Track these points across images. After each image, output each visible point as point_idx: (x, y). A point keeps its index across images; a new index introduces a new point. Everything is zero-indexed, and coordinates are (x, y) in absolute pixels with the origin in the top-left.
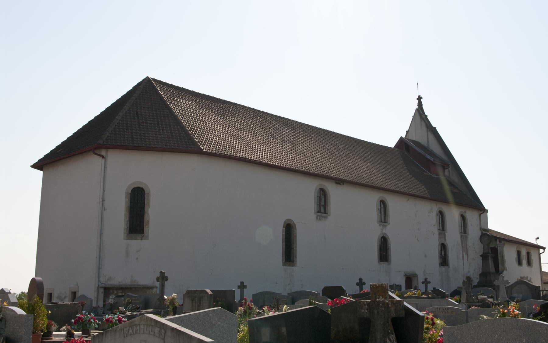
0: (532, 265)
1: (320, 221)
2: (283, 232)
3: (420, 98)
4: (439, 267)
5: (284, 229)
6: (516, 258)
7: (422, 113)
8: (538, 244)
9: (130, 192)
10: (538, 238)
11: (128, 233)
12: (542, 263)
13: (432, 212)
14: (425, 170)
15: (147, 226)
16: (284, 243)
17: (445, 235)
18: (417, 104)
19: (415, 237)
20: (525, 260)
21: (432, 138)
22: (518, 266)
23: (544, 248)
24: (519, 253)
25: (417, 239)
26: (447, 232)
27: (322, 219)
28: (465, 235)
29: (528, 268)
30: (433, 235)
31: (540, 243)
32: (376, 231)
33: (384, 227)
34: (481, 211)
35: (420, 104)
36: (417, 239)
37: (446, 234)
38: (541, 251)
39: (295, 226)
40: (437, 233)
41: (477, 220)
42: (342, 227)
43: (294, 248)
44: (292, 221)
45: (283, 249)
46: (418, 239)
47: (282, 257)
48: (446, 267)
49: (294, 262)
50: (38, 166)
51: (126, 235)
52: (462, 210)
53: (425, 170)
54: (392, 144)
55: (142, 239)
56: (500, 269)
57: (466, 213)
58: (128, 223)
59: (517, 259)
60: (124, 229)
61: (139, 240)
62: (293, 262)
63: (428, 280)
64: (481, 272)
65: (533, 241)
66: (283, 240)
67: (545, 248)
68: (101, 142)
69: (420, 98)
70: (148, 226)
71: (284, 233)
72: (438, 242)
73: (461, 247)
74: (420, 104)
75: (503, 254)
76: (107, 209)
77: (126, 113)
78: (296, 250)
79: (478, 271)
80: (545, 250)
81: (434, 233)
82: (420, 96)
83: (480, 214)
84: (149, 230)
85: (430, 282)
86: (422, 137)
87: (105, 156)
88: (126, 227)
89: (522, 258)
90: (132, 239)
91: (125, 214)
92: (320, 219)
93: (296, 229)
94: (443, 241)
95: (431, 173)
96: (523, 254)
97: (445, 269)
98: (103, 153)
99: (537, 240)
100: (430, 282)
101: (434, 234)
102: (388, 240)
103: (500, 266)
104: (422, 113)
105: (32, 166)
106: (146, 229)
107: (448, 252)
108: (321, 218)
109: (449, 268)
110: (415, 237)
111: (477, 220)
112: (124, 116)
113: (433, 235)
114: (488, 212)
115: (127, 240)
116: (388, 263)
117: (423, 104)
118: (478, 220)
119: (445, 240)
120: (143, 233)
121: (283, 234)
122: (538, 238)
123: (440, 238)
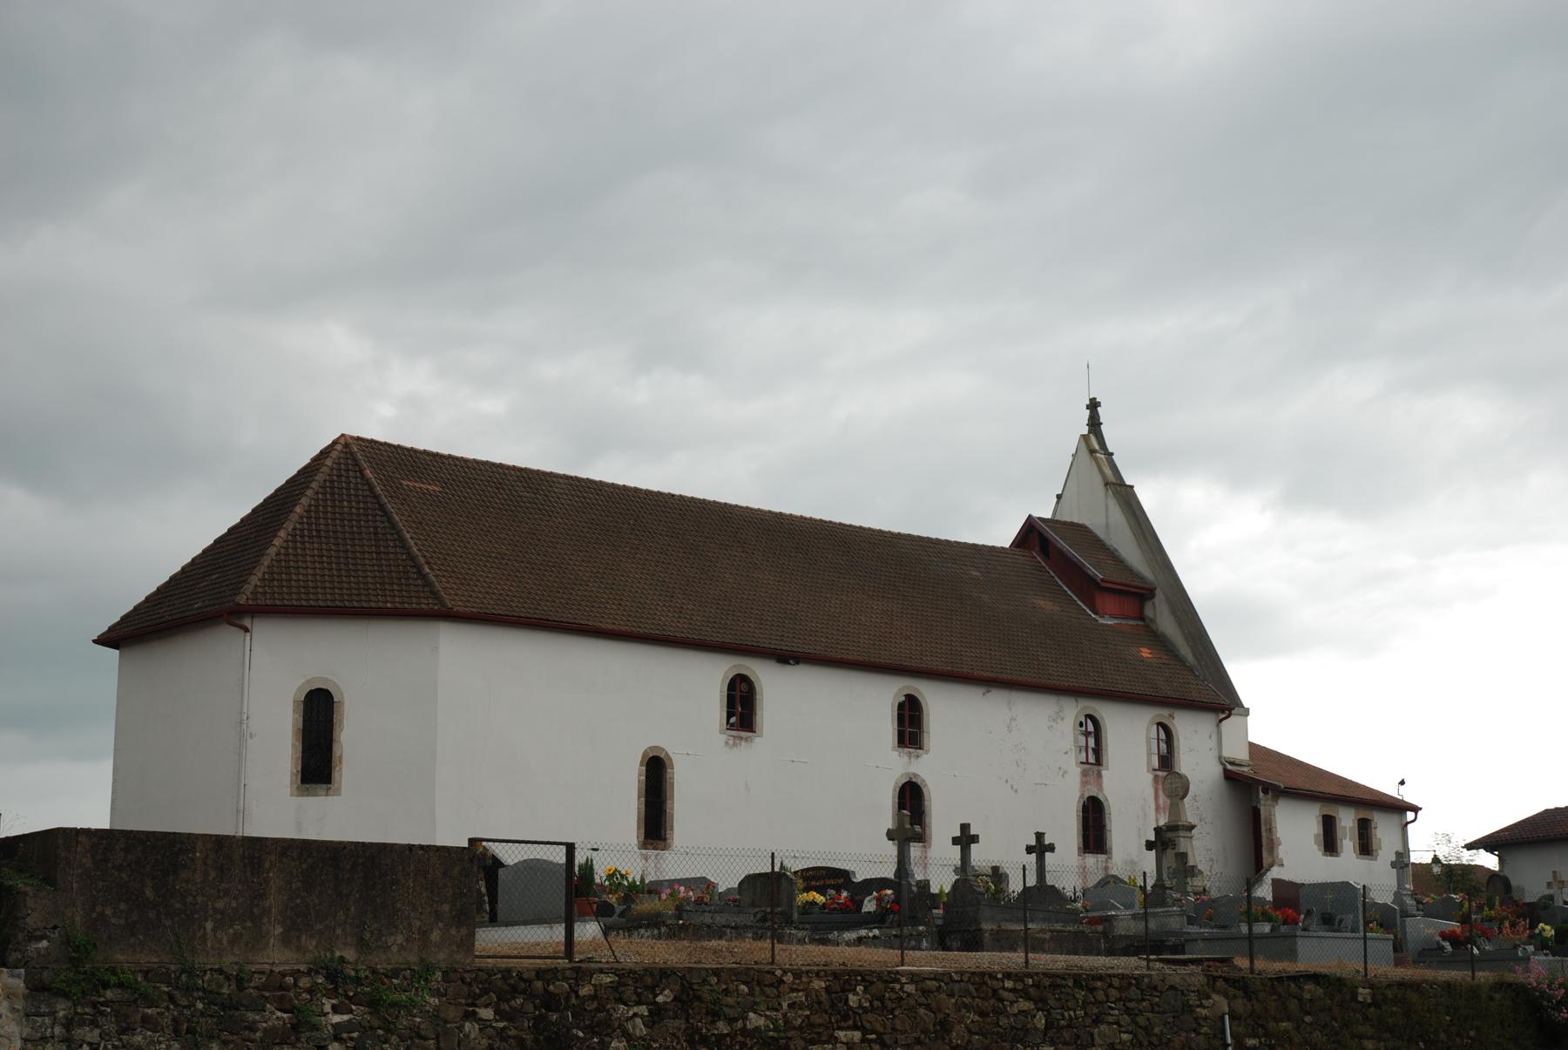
0: (1375, 854)
1: (735, 749)
2: (640, 775)
3: (1093, 405)
4: (1079, 855)
5: (644, 768)
6: (1316, 836)
7: (1097, 447)
8: (1405, 799)
9: (303, 699)
10: (1402, 783)
11: (300, 782)
12: (1411, 848)
13: (1062, 719)
14: (1088, 610)
15: (337, 768)
16: (643, 799)
17: (1099, 775)
18: (1087, 422)
19: (1007, 781)
20: (1351, 840)
21: (1117, 515)
22: (1325, 855)
23: (1416, 809)
24: (1329, 824)
25: (1012, 787)
26: (1107, 769)
27: (740, 745)
28: (1095, 768)
29: (1360, 860)
30: (1063, 776)
31: (1408, 795)
32: (897, 766)
33: (913, 759)
34: (1223, 712)
35: (1094, 423)
36: (1012, 787)
37: (1103, 773)
38: (1410, 815)
39: (671, 760)
40: (1075, 772)
41: (1210, 737)
42: (793, 761)
43: (668, 811)
44: (664, 750)
45: (639, 812)
46: (1015, 787)
47: (639, 828)
48: (1102, 857)
49: (668, 841)
50: (113, 638)
51: (295, 786)
52: (1162, 713)
53: (1088, 610)
54: (1002, 534)
55: (327, 795)
56: (1265, 862)
57: (1173, 718)
58: (300, 762)
59: (1322, 837)
60: (292, 776)
61: (321, 796)
62: (665, 839)
63: (1033, 842)
64: (1535, 900)
65: (1388, 788)
66: (639, 792)
67: (1421, 809)
68: (241, 600)
69: (1093, 405)
70: (341, 768)
71: (643, 778)
72: (1078, 795)
73: (1153, 806)
74: (1094, 423)
75: (1271, 825)
76: (255, 735)
77: (294, 529)
78: (673, 814)
79: (1209, 868)
80: (1420, 813)
81: (1065, 772)
82: (1095, 399)
83: (1221, 721)
84: (341, 776)
85: (1051, 848)
86: (1101, 517)
87: (249, 628)
88: (295, 771)
89: (1339, 834)
90: (308, 795)
91: (293, 745)
92: (734, 745)
93: (673, 769)
94: (1092, 791)
95: (1096, 613)
96: (1343, 824)
97: (1097, 861)
98: (247, 622)
99: (1401, 787)
100: (1051, 848)
101: (1066, 775)
102: (924, 790)
103: (1265, 854)
104: (1097, 447)
105: (95, 641)
106: (336, 775)
107: (1110, 818)
108: (737, 742)
109: (1111, 858)
110: (1007, 781)
111: (1210, 737)
112: (290, 538)
113: (1063, 776)
114: (1248, 715)
115: (298, 796)
116: (921, 844)
117: (1101, 421)
118: (1214, 737)
119: (1100, 787)
120: (330, 782)
121: (639, 781)
122: (1402, 783)
123: (1084, 784)
